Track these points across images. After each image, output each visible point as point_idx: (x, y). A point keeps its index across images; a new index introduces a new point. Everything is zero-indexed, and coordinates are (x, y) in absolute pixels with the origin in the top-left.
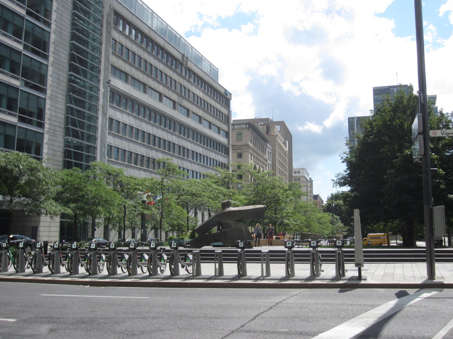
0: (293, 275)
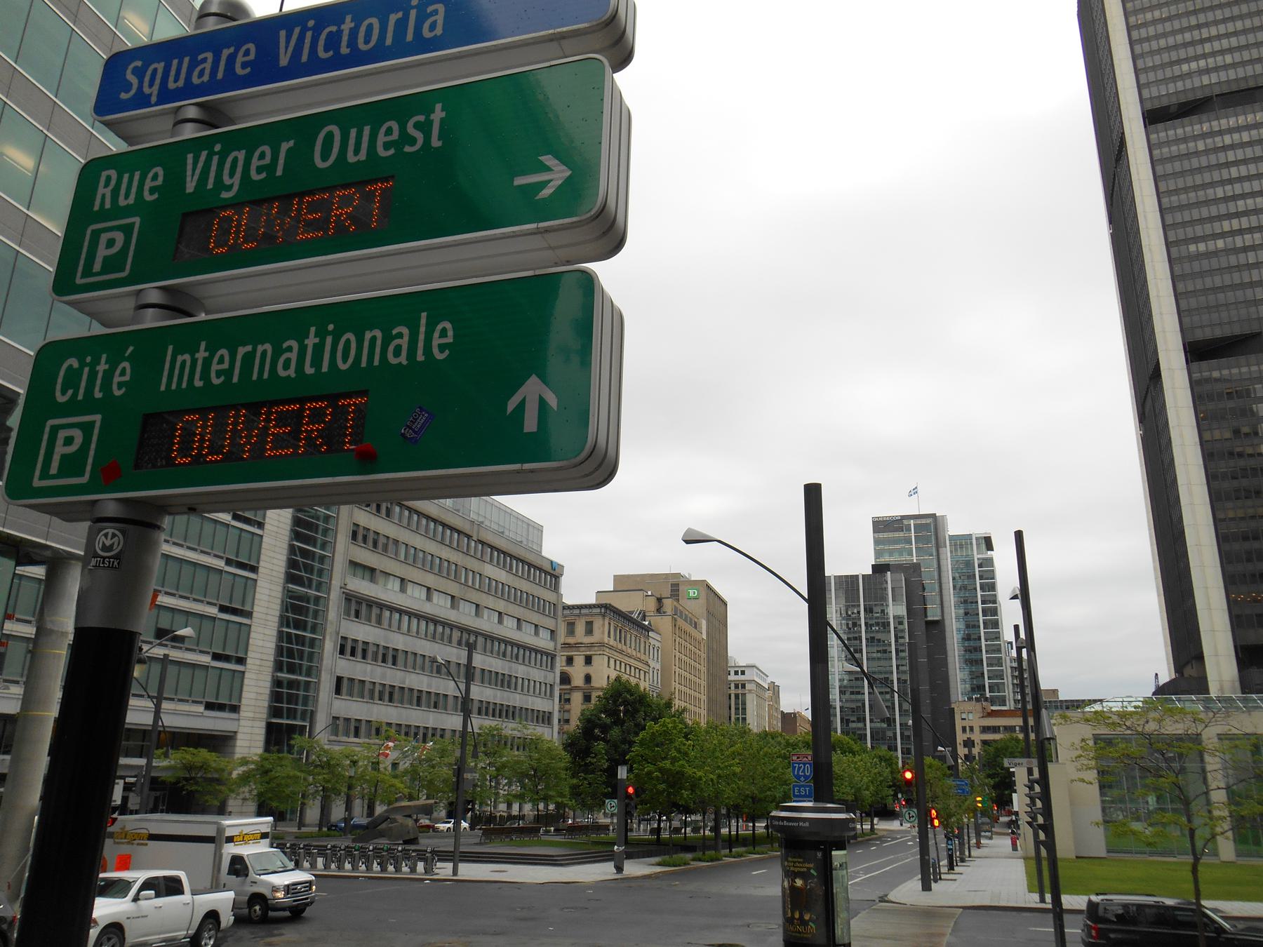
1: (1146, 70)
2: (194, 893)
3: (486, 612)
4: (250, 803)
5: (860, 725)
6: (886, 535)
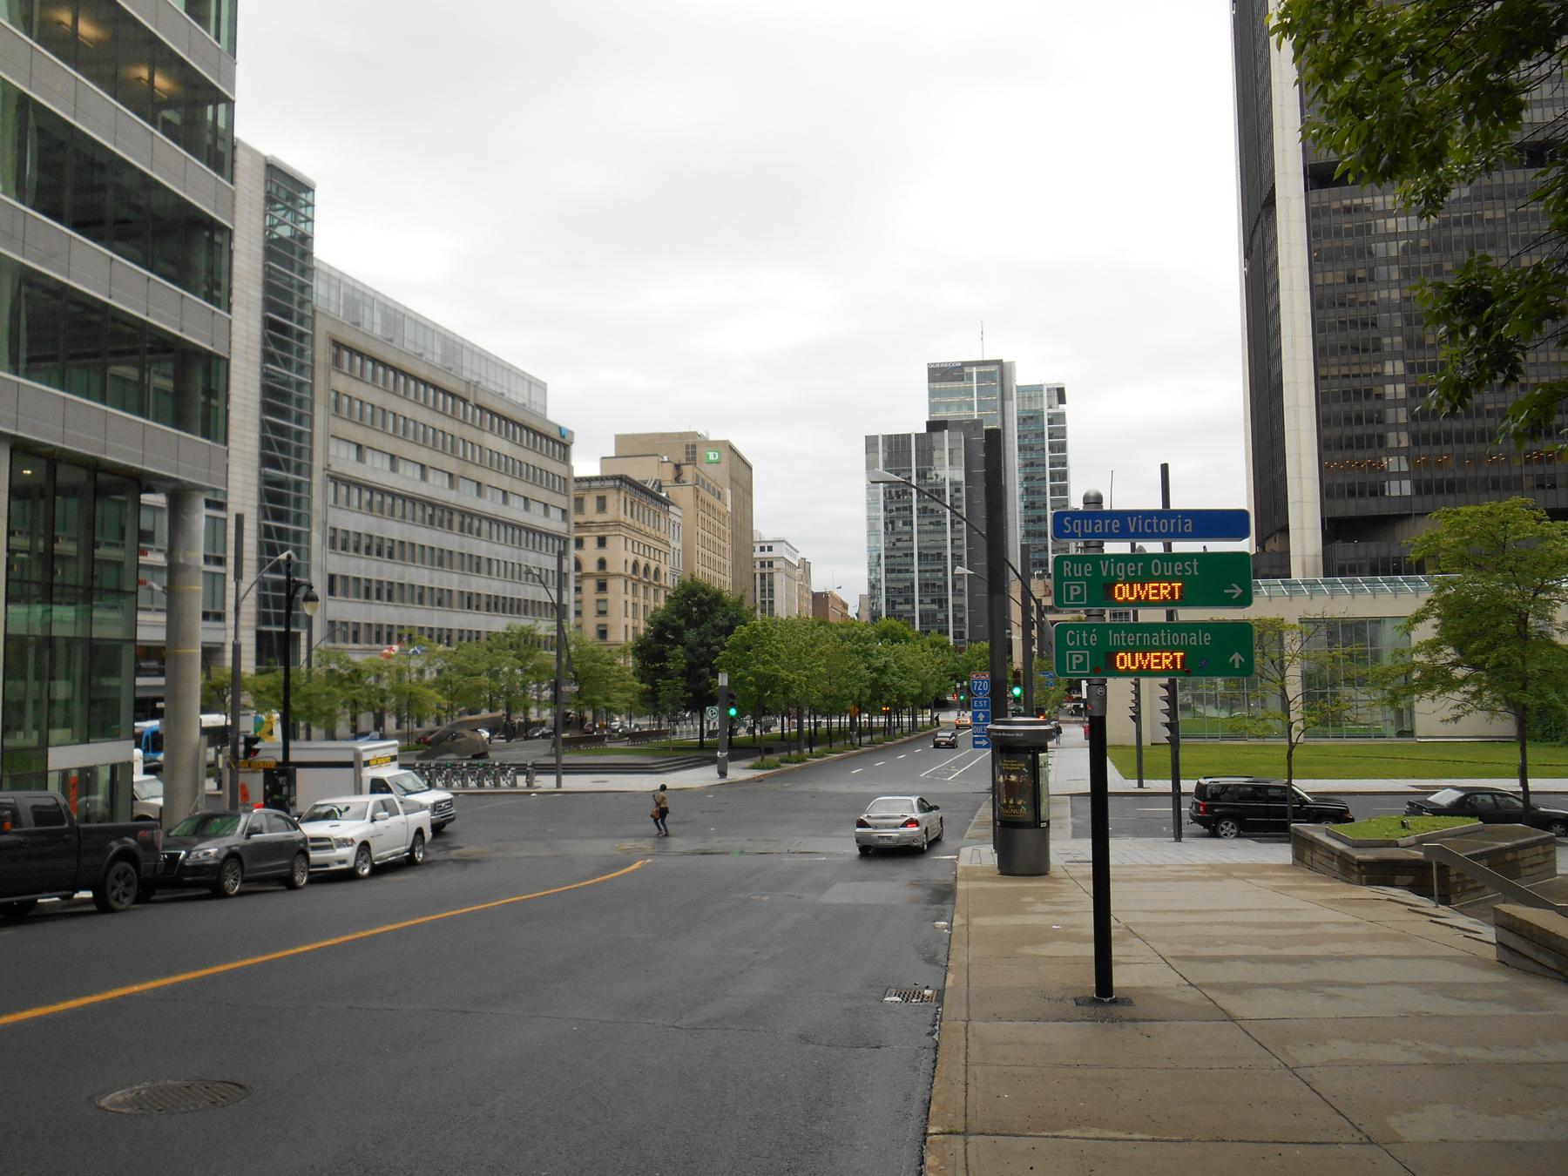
2: (406, 813)
3: (488, 491)
4: (965, 751)
5: (908, 607)
6: (943, 385)
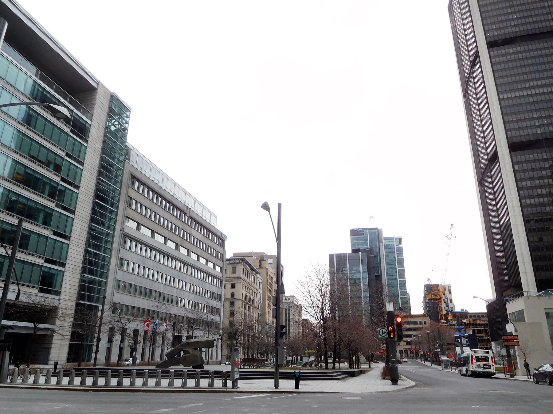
0: (147, 385)
1: (487, 24)
